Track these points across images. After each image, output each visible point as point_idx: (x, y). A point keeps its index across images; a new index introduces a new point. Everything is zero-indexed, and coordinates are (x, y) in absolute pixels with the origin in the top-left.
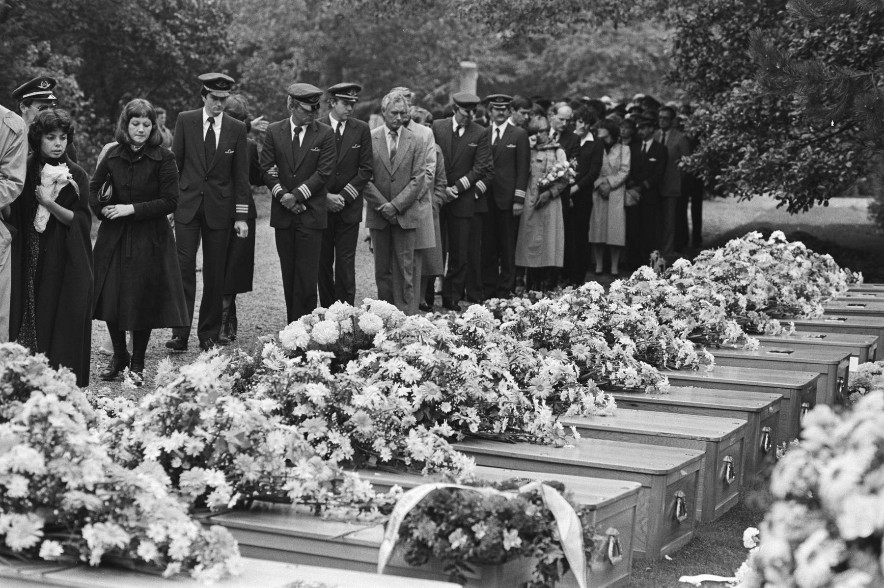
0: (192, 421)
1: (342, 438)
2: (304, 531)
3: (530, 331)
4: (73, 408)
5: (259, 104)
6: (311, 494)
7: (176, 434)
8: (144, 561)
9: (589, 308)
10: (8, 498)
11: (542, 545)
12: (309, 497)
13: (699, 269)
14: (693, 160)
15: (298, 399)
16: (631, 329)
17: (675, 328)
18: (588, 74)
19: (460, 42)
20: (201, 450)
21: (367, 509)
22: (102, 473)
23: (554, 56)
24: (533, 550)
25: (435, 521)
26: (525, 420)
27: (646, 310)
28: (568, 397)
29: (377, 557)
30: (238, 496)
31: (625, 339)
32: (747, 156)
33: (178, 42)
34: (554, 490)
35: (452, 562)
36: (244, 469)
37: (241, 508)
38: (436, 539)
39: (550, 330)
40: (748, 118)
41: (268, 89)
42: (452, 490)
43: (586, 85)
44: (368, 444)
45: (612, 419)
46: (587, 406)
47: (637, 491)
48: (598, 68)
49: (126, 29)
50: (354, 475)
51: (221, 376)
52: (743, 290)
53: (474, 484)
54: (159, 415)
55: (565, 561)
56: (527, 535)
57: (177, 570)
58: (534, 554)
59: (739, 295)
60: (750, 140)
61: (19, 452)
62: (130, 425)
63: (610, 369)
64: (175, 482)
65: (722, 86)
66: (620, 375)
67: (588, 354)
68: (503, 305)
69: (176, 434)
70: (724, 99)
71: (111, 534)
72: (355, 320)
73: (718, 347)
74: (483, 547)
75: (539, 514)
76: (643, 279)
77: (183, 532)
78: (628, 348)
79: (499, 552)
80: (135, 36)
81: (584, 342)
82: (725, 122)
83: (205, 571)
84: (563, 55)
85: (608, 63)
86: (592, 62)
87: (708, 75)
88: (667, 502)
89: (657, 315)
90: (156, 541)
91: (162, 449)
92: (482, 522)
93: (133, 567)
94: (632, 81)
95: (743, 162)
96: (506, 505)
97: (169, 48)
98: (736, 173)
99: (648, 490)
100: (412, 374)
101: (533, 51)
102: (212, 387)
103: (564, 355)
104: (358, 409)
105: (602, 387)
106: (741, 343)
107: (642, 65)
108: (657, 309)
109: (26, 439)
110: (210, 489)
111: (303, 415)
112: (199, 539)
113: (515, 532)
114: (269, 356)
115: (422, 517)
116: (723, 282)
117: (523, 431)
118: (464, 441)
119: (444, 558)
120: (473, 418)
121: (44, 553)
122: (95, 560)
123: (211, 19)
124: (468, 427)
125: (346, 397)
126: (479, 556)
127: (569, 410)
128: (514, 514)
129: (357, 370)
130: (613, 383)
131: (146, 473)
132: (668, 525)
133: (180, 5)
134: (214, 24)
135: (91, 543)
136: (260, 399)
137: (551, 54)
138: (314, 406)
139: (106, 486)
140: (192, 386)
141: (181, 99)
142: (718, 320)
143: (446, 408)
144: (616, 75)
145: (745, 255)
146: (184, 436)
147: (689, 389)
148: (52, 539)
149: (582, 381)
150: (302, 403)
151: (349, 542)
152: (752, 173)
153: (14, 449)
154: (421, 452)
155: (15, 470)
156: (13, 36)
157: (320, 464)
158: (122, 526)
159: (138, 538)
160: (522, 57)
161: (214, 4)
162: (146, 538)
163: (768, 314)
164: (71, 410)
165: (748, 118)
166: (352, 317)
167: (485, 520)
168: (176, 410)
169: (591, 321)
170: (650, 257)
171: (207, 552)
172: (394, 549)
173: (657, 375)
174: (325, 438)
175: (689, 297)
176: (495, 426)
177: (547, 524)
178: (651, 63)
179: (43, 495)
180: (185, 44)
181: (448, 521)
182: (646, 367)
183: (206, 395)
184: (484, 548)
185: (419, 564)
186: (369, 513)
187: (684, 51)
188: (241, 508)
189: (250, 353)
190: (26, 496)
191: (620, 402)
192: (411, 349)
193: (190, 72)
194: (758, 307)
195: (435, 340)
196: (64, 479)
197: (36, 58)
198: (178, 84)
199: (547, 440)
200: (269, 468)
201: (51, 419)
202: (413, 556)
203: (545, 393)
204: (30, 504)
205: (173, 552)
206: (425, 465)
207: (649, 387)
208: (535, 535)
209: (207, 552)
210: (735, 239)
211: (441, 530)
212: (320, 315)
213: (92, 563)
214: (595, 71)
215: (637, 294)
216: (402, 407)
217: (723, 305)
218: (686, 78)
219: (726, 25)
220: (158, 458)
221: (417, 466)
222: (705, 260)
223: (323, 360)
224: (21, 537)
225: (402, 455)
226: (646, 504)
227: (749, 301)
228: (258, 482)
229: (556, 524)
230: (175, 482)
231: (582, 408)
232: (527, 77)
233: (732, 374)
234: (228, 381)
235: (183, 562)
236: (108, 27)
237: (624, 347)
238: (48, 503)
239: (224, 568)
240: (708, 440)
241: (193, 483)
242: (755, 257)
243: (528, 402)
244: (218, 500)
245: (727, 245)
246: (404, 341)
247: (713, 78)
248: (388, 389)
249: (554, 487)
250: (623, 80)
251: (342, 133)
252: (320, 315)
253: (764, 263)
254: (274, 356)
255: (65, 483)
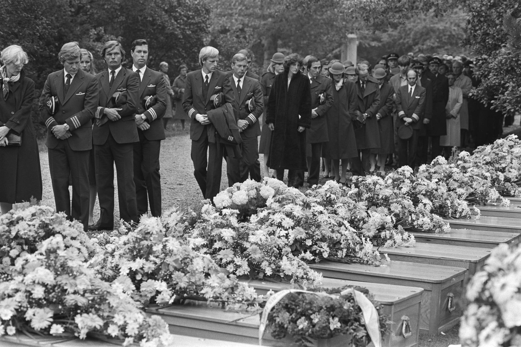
0: (150, 251)
1: (243, 261)
2: (213, 318)
3: (365, 196)
4: (80, 244)
5: (225, 62)
6: (218, 295)
7: (138, 260)
8: (112, 336)
9: (404, 182)
10: (33, 299)
11: (353, 327)
12: (218, 298)
13: (476, 157)
14: (478, 92)
15: (216, 238)
16: (429, 195)
17: (458, 193)
18: (425, 40)
19: (347, 22)
20: (153, 269)
21: (252, 305)
22: (89, 283)
23: (404, 30)
24: (347, 330)
25: (289, 312)
26: (357, 250)
27: (441, 183)
28: (386, 236)
29: (258, 334)
30: (175, 296)
31: (426, 200)
32: (510, 89)
33: (178, 25)
34: (362, 294)
35: (300, 337)
36: (178, 280)
37: (177, 304)
38: (289, 323)
39: (378, 195)
40: (511, 66)
41: (231, 53)
42: (299, 293)
43: (425, 47)
44: (258, 265)
45: (413, 249)
46: (397, 241)
47: (421, 293)
48: (431, 37)
49: (148, 19)
50: (245, 284)
51: (176, 224)
52: (503, 170)
53: (314, 290)
54: (129, 249)
55: (368, 337)
56: (344, 321)
57: (132, 342)
58: (348, 333)
59: (499, 173)
60: (512, 79)
61: (39, 271)
62: (112, 254)
63: (414, 219)
64: (138, 288)
65: (496, 47)
66: (420, 222)
67: (400, 209)
68: (360, 179)
69: (138, 260)
70: (497, 54)
71: (92, 320)
72: (258, 190)
73: (485, 205)
74: (317, 328)
75: (352, 308)
76: (439, 164)
77: (134, 318)
78: (427, 206)
79: (326, 332)
80: (153, 23)
81: (397, 202)
82: (496, 69)
83: (148, 343)
84: (410, 29)
85: (437, 33)
86: (427, 33)
87: (487, 41)
88: (442, 301)
89: (447, 185)
90: (119, 325)
91: (130, 269)
92: (317, 313)
93: (106, 340)
94: (451, 44)
95: (508, 92)
96: (331, 303)
97: (173, 29)
98: (503, 99)
99: (429, 293)
100: (288, 222)
101: (391, 27)
102: (161, 231)
103: (386, 210)
104: (252, 244)
105: (406, 230)
106: (499, 202)
107: (458, 34)
108: (448, 182)
109: (44, 263)
110: (158, 292)
111: (220, 248)
112: (145, 323)
113: (337, 319)
114: (206, 212)
115: (281, 310)
116: (491, 165)
117: (356, 257)
118: (320, 262)
119: (294, 335)
120: (325, 250)
121: (52, 331)
122: (83, 335)
123: (197, 12)
124: (322, 254)
125: (244, 236)
126: (315, 334)
127: (386, 244)
128: (336, 308)
129: (256, 220)
130: (416, 227)
131: (120, 283)
132: (443, 313)
133: (180, 4)
134: (199, 15)
135: (80, 325)
136: (194, 238)
137: (402, 29)
138: (226, 242)
139: (92, 292)
140: (149, 231)
141: (180, 59)
142: (485, 188)
143: (309, 243)
144: (442, 41)
145: (505, 149)
146: (143, 261)
147: (464, 230)
148: (57, 323)
149: (395, 227)
150: (219, 241)
151: (240, 324)
152: (513, 99)
153: (36, 269)
154: (290, 270)
155: (36, 282)
156: (81, 24)
157: (224, 277)
158: (99, 316)
159: (108, 322)
160: (385, 31)
161: (199, 3)
162: (113, 323)
163: (518, 185)
164: (78, 245)
165: (511, 66)
166: (256, 188)
167: (319, 311)
168: (139, 245)
169: (405, 190)
170: (451, 150)
171: (150, 331)
172: (265, 329)
173: (443, 222)
174: (232, 262)
175: (468, 175)
176: (338, 254)
177: (357, 314)
178: (464, 34)
179: (53, 297)
180: (182, 27)
181: (296, 312)
182: (436, 217)
183: (157, 236)
184: (318, 329)
185: (280, 338)
186: (253, 307)
187: (473, 26)
188: (177, 304)
189: (195, 210)
190: (42, 298)
191: (418, 239)
192: (288, 207)
193: (185, 43)
194: (512, 180)
195: (303, 202)
196: (65, 288)
197: (95, 37)
198: (178, 50)
199: (370, 262)
200: (193, 280)
201: (58, 252)
202: (277, 333)
203: (372, 234)
204: (45, 302)
205: (128, 331)
206: (292, 278)
207: (438, 229)
208: (349, 321)
209: (150, 331)
210: (499, 139)
211: (292, 318)
212: (237, 187)
213: (81, 337)
214: (429, 39)
215: (435, 173)
216: (278, 243)
217: (489, 179)
218: (474, 42)
219: (498, 10)
220: (128, 274)
221: (288, 278)
222: (480, 152)
223: (232, 214)
224: (40, 322)
225: (279, 271)
226: (429, 301)
227: (505, 176)
228: (187, 288)
229: (362, 314)
230: (138, 288)
231: (395, 242)
232: (388, 43)
233: (493, 221)
234: (180, 227)
235: (135, 337)
236: (138, 18)
237: (425, 205)
238: (56, 301)
239: (159, 340)
240: (470, 261)
241: (148, 289)
242: (512, 150)
243: (358, 239)
244: (162, 299)
245: (495, 142)
246: (284, 203)
247: (490, 42)
248: (274, 232)
249: (362, 292)
250: (446, 44)
251: (209, 82)
252: (237, 187)
253: (517, 153)
254: (209, 213)
255: (66, 290)
